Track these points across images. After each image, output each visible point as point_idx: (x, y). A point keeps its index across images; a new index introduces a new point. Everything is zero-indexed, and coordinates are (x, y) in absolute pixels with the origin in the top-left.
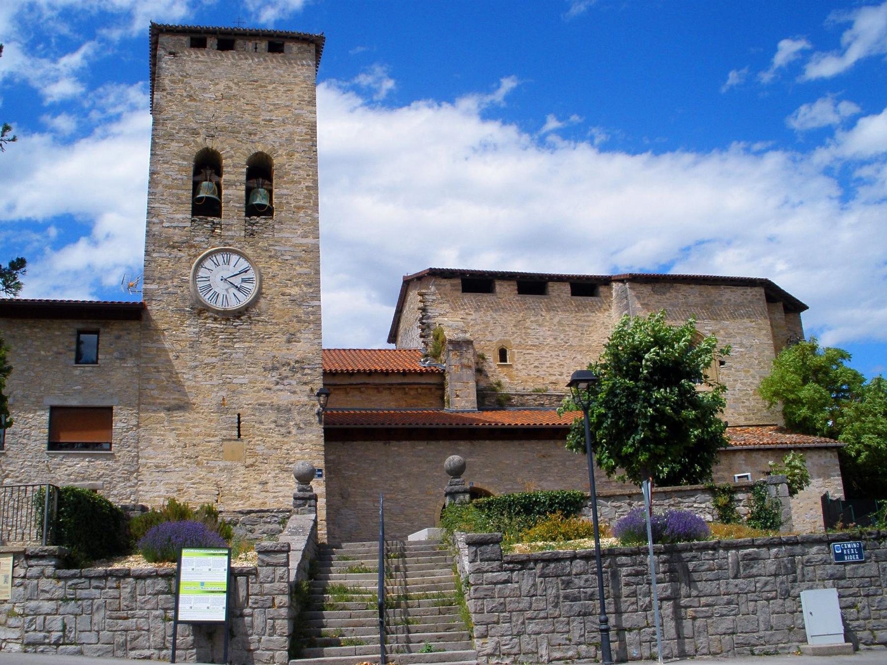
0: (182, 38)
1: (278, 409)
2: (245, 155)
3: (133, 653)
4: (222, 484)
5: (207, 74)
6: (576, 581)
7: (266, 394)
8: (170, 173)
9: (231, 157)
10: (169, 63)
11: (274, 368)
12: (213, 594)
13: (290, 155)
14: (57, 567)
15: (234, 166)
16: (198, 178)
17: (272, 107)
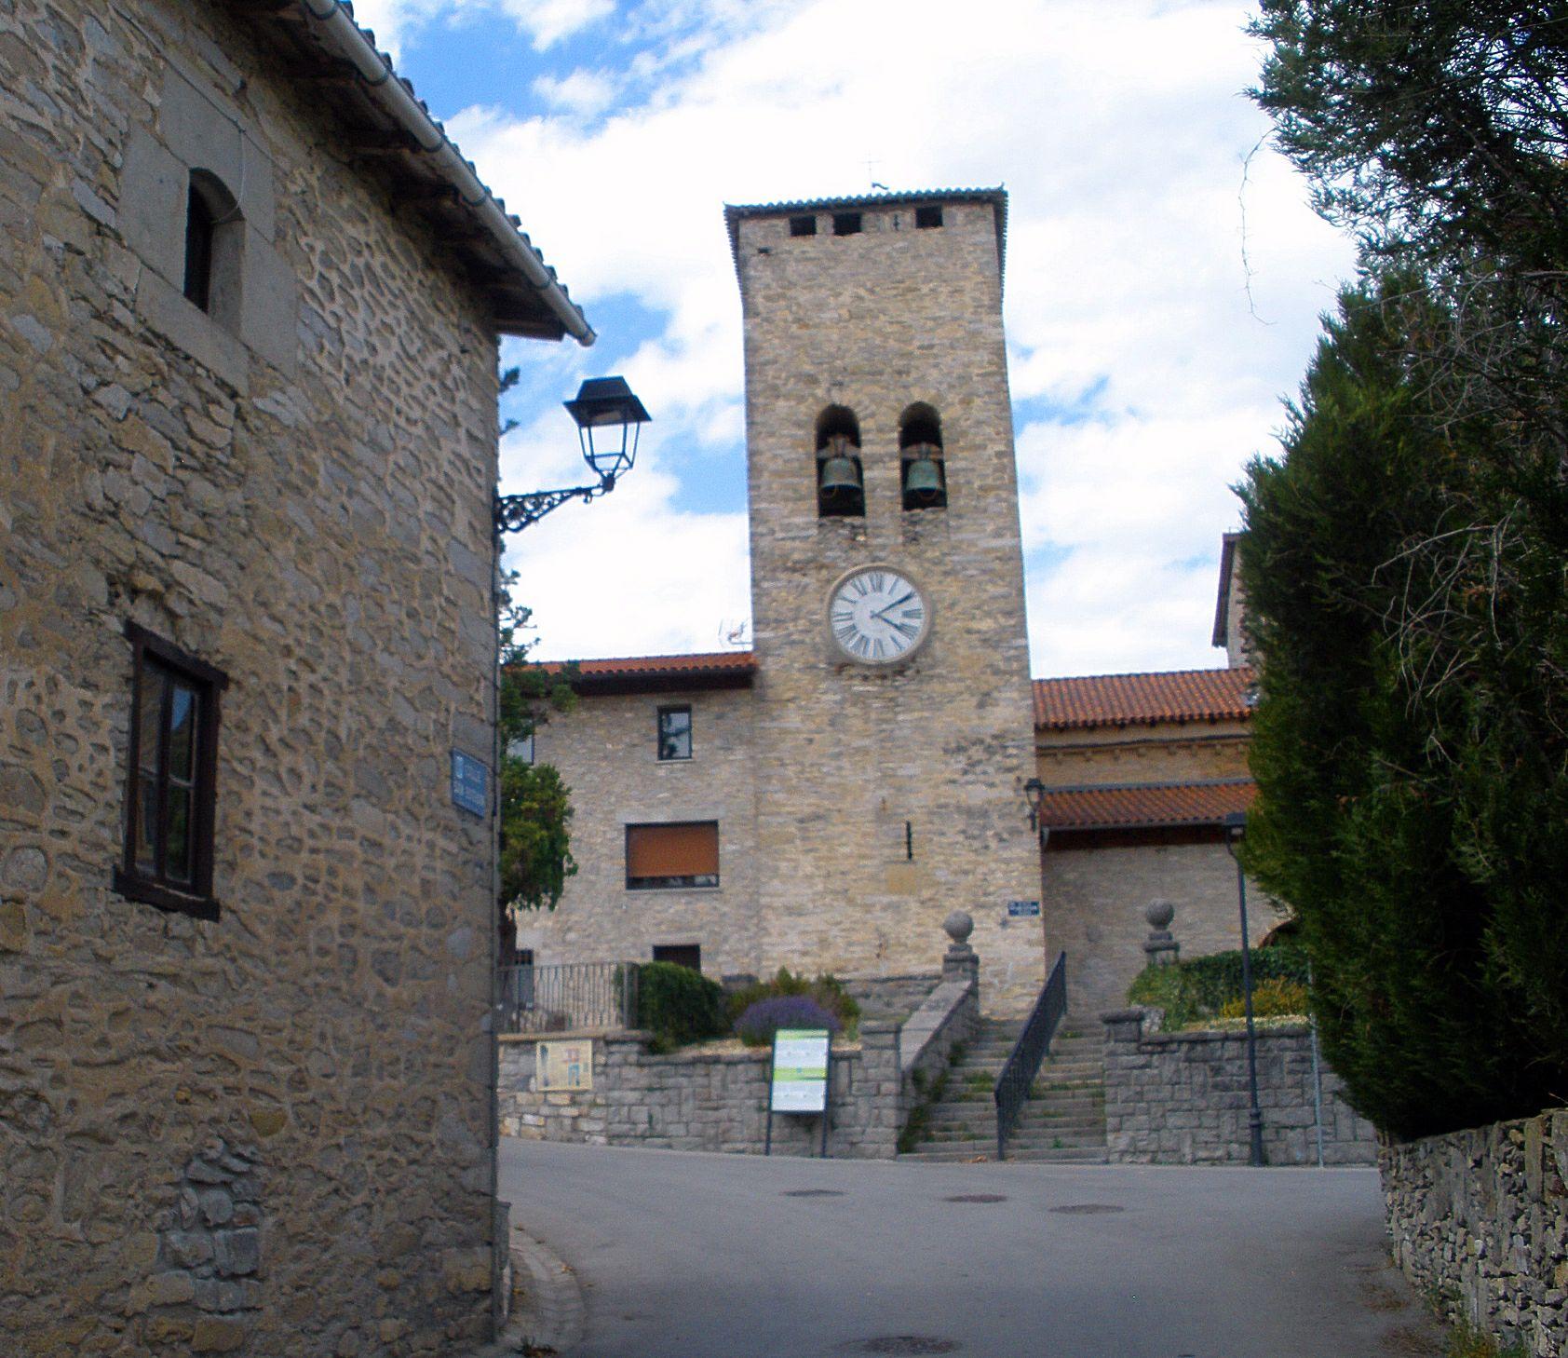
0: (775, 222)
1: (969, 812)
2: (894, 409)
3: (726, 1146)
4: (885, 930)
5: (822, 280)
6: (1228, 1068)
7: (950, 789)
8: (781, 452)
9: (873, 415)
10: (760, 268)
11: (960, 749)
12: (809, 1082)
13: (966, 402)
14: (640, 1053)
15: (880, 430)
16: (824, 453)
17: (930, 324)
